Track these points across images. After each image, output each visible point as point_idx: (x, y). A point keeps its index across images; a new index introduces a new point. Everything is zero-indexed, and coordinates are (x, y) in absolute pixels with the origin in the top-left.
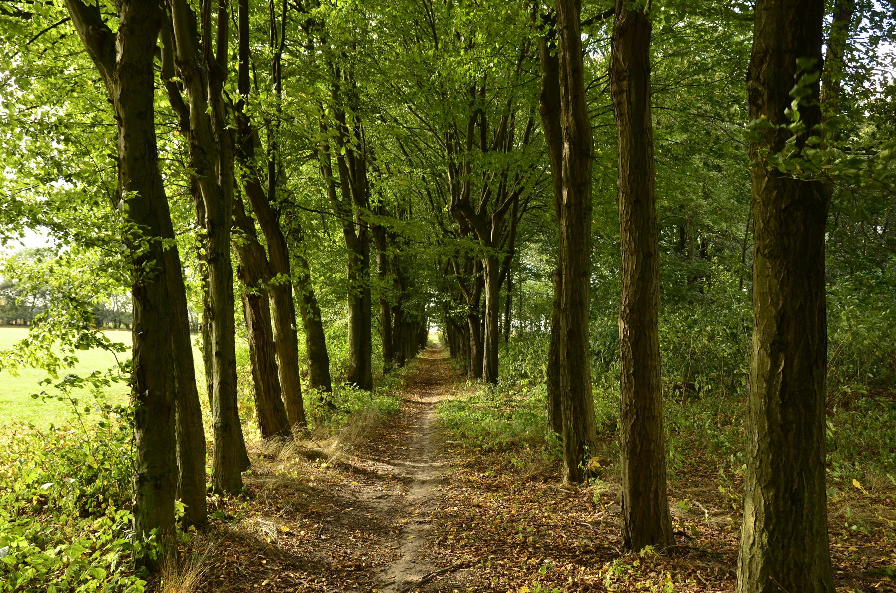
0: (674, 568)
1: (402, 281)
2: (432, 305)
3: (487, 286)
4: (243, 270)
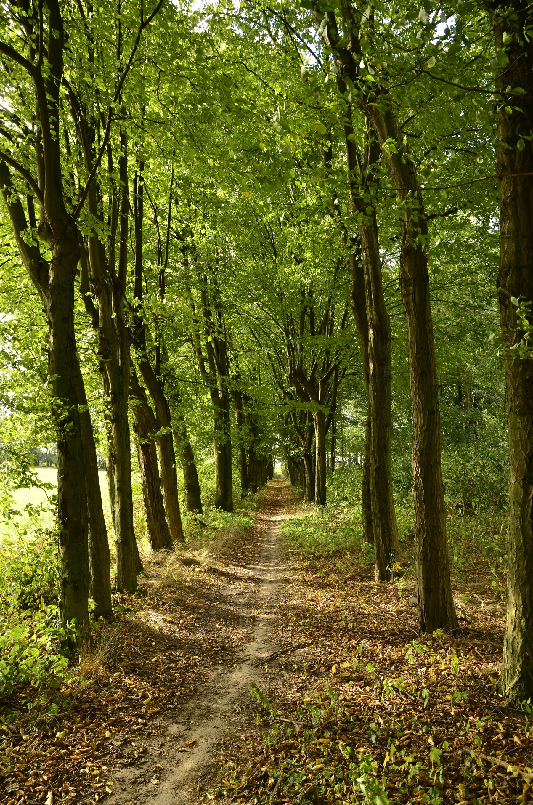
0: (458, 645)
1: (254, 430)
2: (277, 446)
3: (317, 433)
4: (137, 426)
